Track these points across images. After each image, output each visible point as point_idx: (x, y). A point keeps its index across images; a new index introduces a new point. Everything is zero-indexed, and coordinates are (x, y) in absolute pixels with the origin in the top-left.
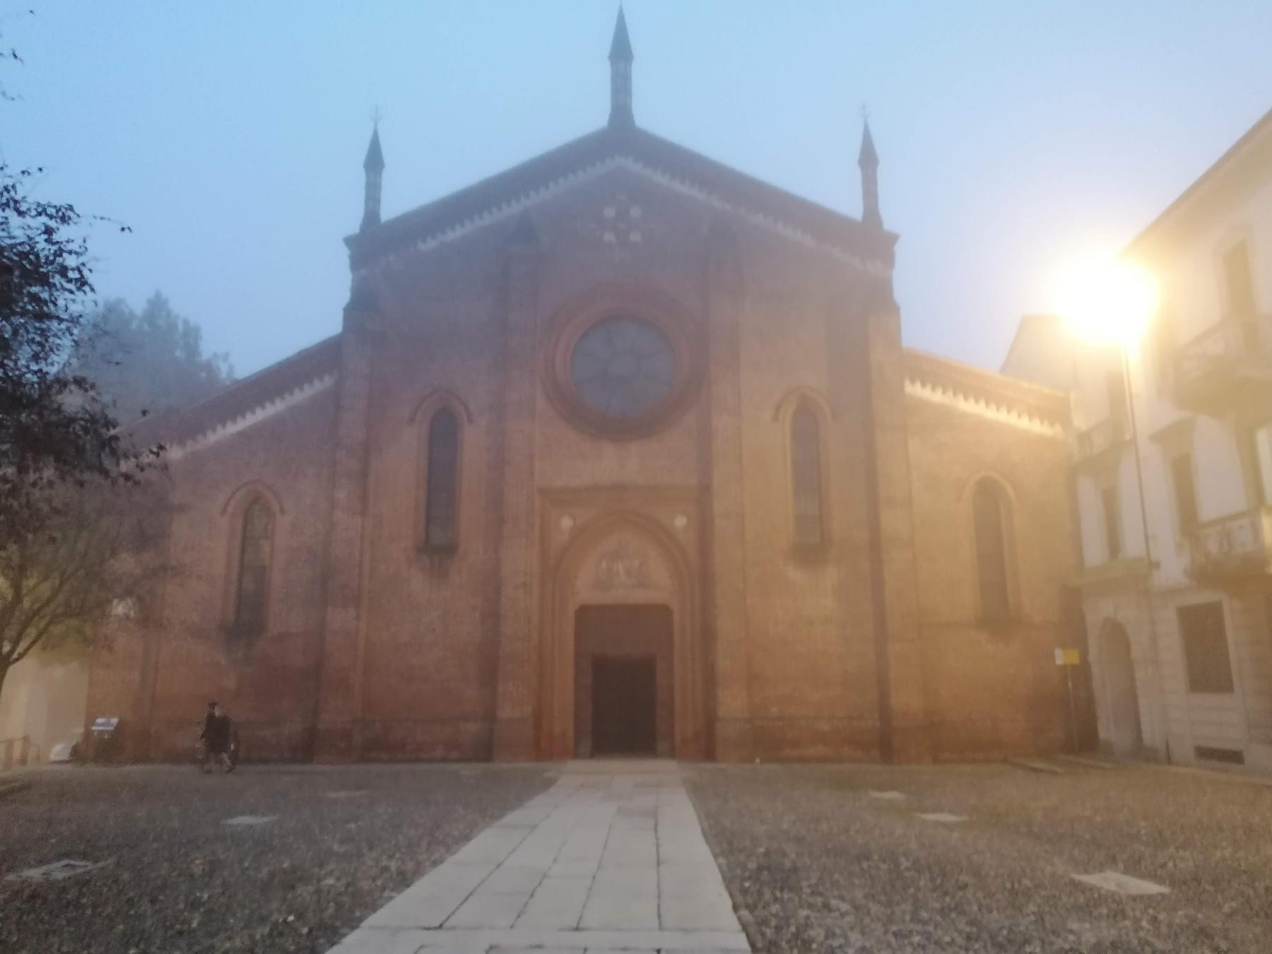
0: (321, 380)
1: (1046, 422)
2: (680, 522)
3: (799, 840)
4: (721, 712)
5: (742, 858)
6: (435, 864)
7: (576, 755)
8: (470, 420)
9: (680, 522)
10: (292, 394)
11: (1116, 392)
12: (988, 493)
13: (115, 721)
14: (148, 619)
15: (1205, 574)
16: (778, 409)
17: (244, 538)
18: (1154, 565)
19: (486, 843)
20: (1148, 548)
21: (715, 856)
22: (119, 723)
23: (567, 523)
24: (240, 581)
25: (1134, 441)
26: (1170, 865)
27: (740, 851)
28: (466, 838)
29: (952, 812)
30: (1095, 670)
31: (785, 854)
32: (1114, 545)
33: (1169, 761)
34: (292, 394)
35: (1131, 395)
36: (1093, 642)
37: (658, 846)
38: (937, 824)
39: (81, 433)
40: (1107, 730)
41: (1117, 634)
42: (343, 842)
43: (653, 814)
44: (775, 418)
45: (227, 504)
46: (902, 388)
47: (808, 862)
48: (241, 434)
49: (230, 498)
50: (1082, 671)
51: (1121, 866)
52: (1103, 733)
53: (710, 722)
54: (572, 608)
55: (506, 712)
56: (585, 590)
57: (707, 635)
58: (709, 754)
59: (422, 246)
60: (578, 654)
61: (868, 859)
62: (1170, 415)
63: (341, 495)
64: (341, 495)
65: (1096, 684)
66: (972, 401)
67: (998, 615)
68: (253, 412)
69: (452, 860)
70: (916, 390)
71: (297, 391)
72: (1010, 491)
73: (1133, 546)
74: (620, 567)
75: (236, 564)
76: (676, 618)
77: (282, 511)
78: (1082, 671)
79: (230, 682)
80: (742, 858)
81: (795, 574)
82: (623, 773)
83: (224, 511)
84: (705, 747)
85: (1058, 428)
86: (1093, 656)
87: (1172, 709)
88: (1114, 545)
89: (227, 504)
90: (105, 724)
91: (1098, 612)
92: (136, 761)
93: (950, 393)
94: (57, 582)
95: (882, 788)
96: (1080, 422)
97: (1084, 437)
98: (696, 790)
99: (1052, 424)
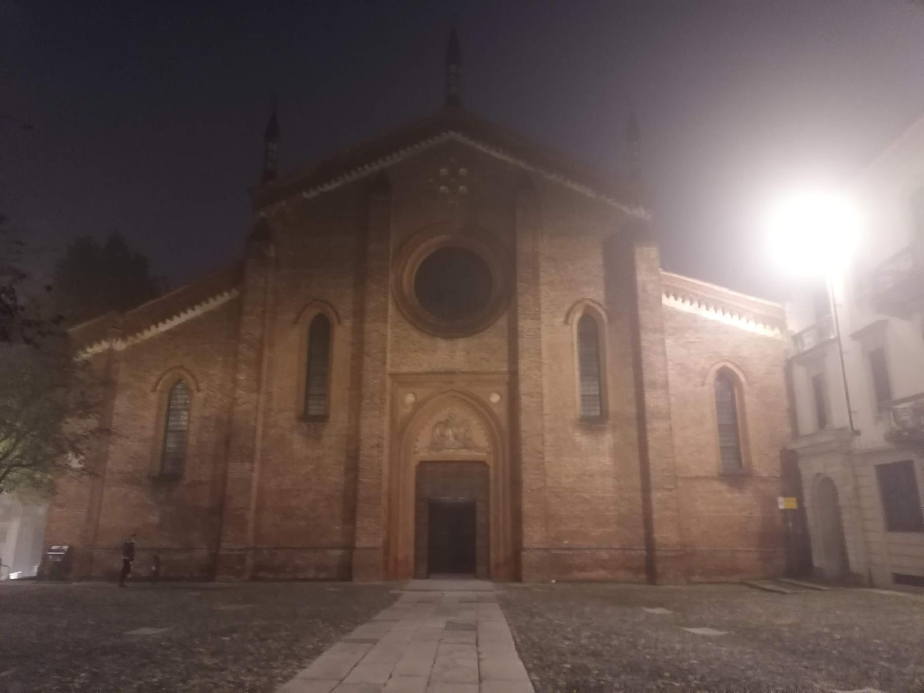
0: (229, 292)
1: (768, 327)
2: (495, 398)
3: (596, 655)
4: (526, 543)
5: (551, 674)
6: (286, 679)
7: (416, 576)
8: (339, 323)
9: (495, 398)
10: (207, 302)
11: (821, 308)
12: (726, 379)
13: (65, 547)
14: (93, 471)
15: (898, 438)
16: (568, 315)
17: (169, 410)
18: (857, 433)
19: (334, 656)
20: (851, 421)
21: (529, 671)
22: (69, 549)
23: (410, 399)
24: (165, 442)
25: (838, 339)
26: (917, 680)
27: (550, 667)
28: (318, 652)
29: (712, 627)
30: (810, 514)
31: (588, 671)
32: (822, 419)
33: (872, 585)
34: (207, 302)
35: (835, 305)
36: (808, 494)
37: (479, 660)
38: (705, 638)
39: (893, 667)
40: (818, 560)
41: (827, 485)
42: (214, 654)
43: (473, 628)
44: (566, 322)
45: (157, 384)
46: (660, 300)
47: (610, 678)
48: (168, 332)
49: (159, 380)
50: (799, 514)
51: (877, 683)
52: (817, 562)
53: (517, 549)
54: (413, 463)
55: (362, 542)
56: (422, 448)
57: (515, 483)
58: (516, 576)
59: (306, 195)
60: (418, 498)
61: (661, 676)
62: (868, 319)
63: (241, 377)
64: (241, 377)
65: (811, 523)
66: (712, 310)
67: (736, 473)
68: (179, 316)
69: (302, 673)
70: (669, 302)
71: (211, 300)
72: (742, 379)
73: (838, 418)
74: (449, 432)
75: (162, 430)
76: (492, 471)
77: (198, 390)
78: (799, 514)
79: (154, 519)
80: (551, 674)
81: (580, 438)
82: (452, 589)
83: (154, 390)
84: (513, 570)
85: (777, 331)
86: (807, 503)
87: (870, 540)
88: (822, 419)
89: (157, 384)
90: (59, 550)
91: (810, 469)
92: (80, 579)
93: (696, 305)
94: (14, 440)
95: (651, 605)
96: (794, 326)
97: (797, 338)
98: (506, 605)
99: (772, 328)
